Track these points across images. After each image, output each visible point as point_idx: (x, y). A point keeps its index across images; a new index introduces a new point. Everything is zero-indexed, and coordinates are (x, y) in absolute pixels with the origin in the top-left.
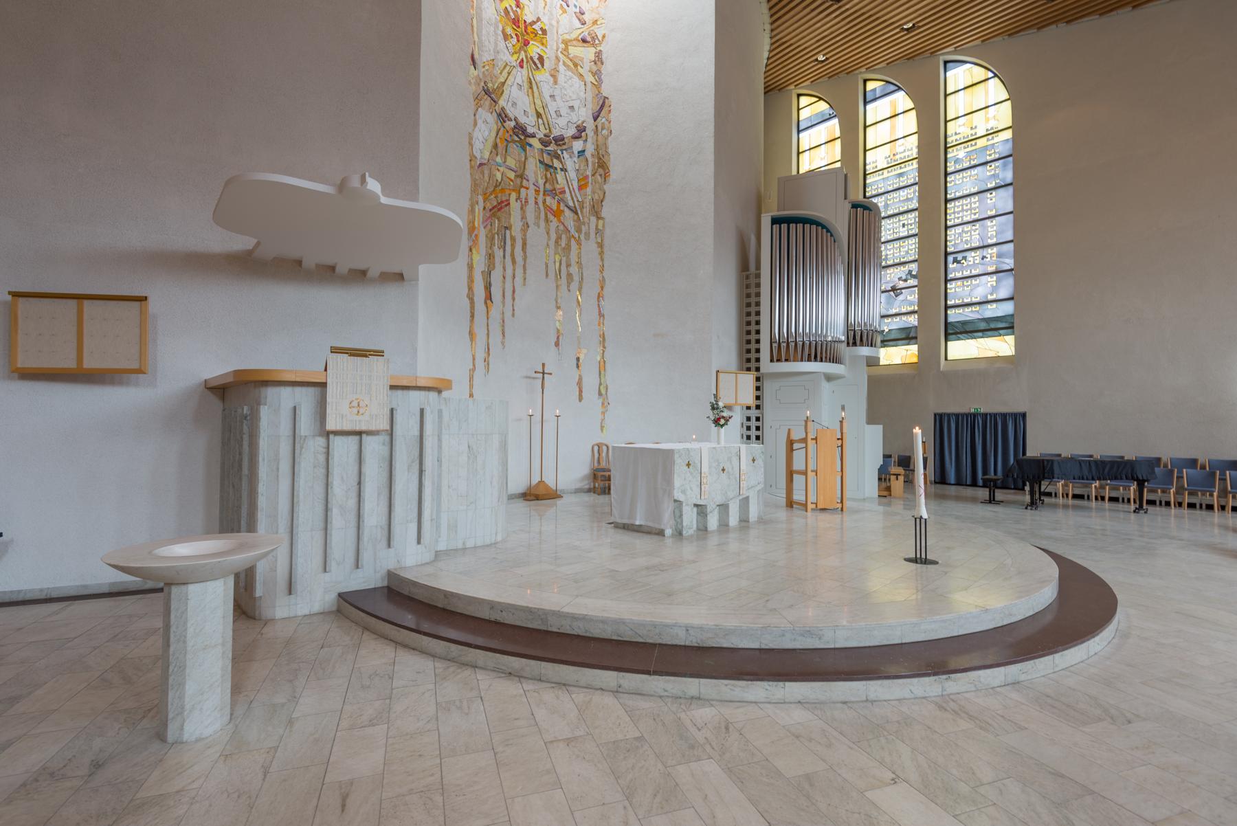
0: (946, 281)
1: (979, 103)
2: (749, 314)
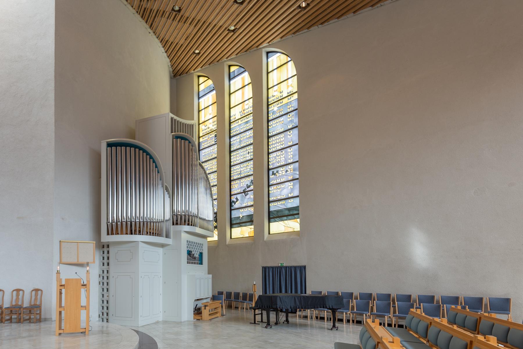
0: (269, 186)
1: (282, 74)
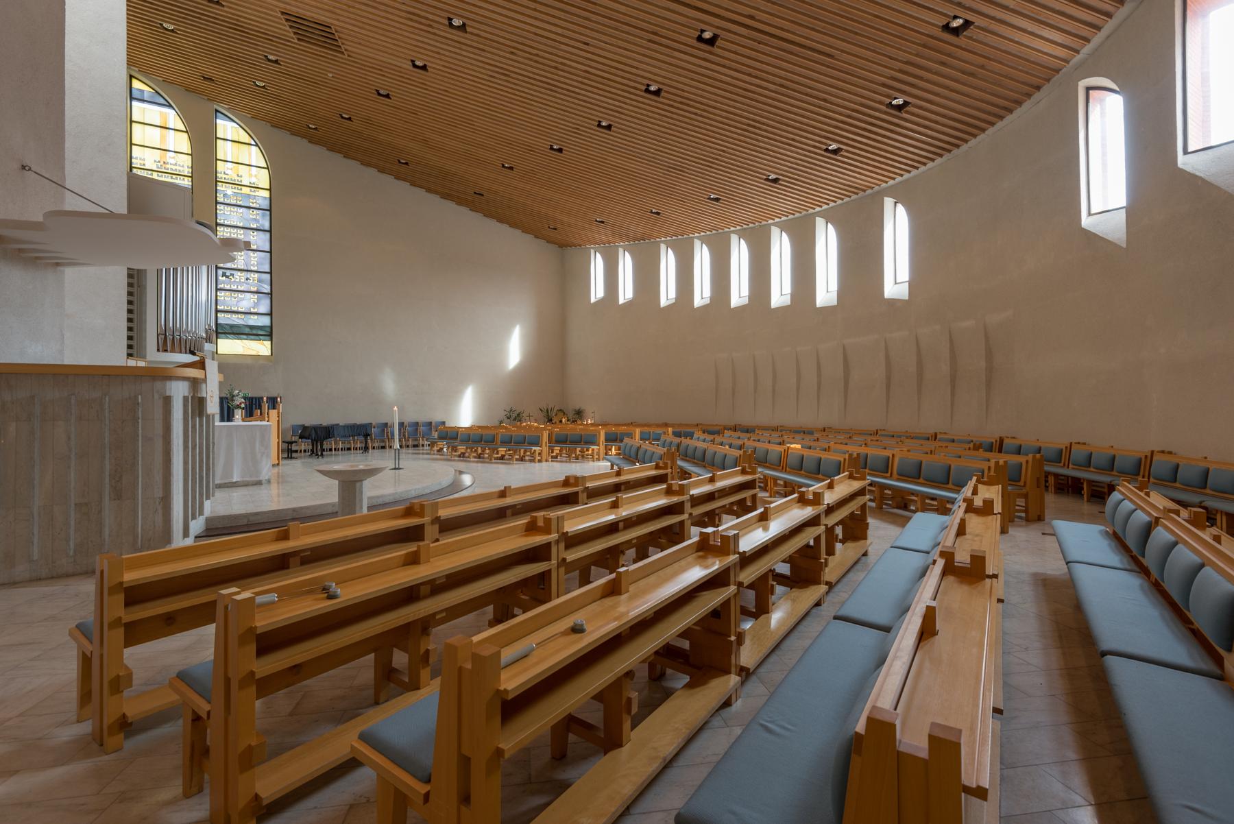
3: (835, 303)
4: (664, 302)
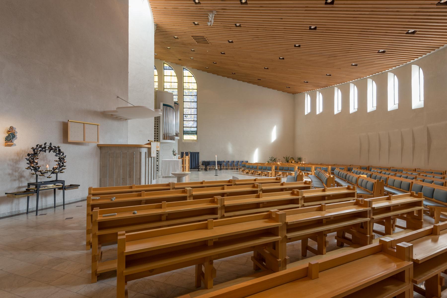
2: (157, 129)
3: (423, 106)
4: (336, 112)
